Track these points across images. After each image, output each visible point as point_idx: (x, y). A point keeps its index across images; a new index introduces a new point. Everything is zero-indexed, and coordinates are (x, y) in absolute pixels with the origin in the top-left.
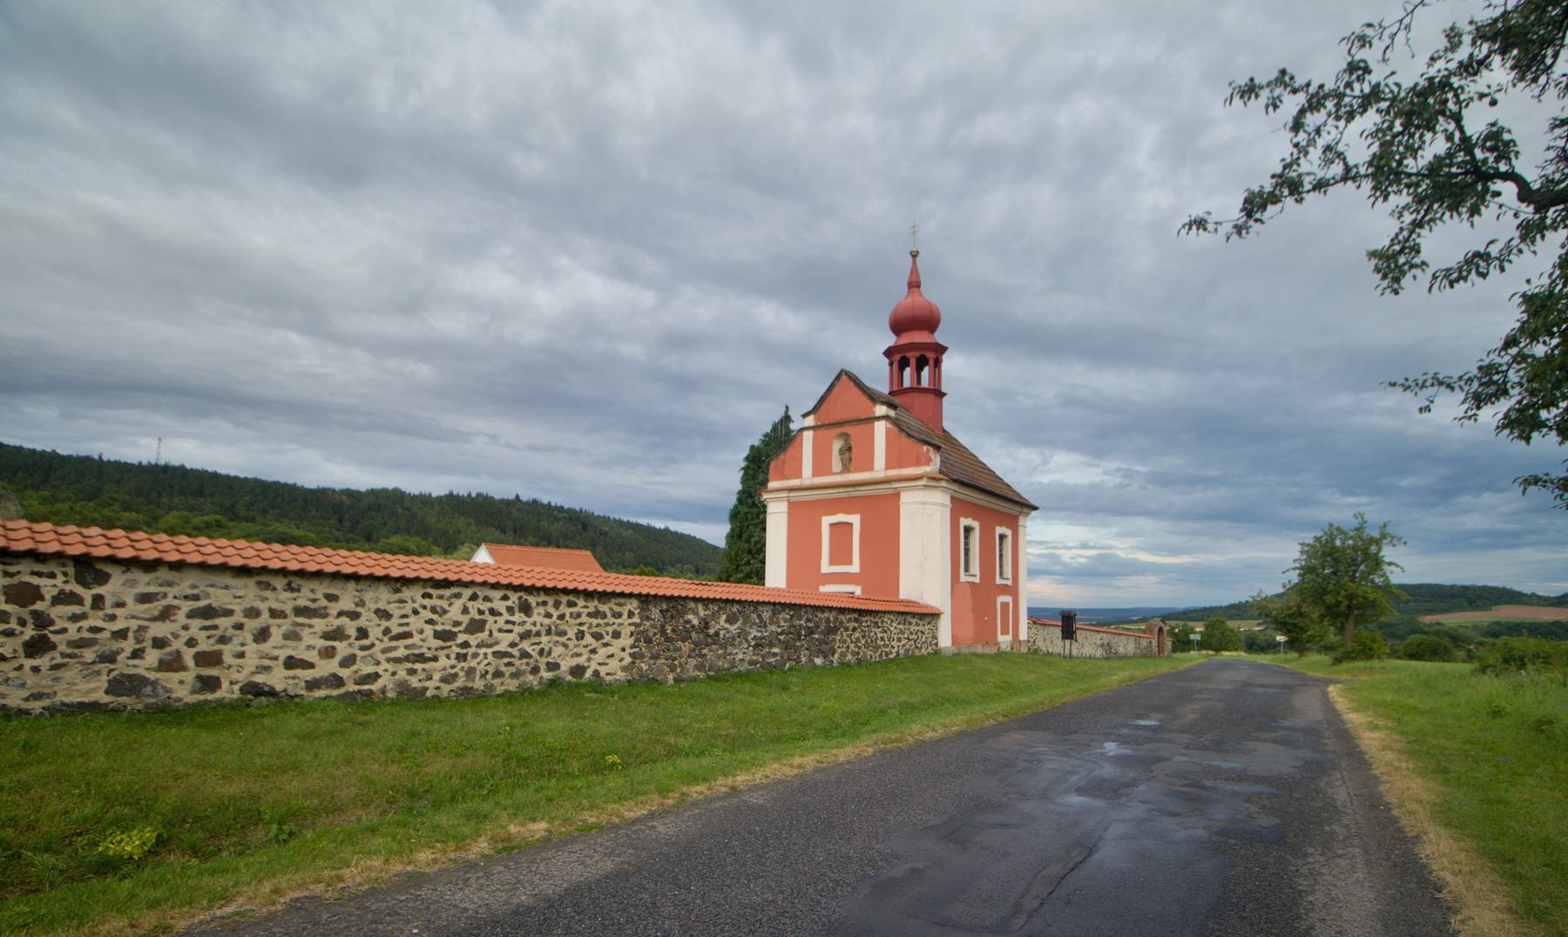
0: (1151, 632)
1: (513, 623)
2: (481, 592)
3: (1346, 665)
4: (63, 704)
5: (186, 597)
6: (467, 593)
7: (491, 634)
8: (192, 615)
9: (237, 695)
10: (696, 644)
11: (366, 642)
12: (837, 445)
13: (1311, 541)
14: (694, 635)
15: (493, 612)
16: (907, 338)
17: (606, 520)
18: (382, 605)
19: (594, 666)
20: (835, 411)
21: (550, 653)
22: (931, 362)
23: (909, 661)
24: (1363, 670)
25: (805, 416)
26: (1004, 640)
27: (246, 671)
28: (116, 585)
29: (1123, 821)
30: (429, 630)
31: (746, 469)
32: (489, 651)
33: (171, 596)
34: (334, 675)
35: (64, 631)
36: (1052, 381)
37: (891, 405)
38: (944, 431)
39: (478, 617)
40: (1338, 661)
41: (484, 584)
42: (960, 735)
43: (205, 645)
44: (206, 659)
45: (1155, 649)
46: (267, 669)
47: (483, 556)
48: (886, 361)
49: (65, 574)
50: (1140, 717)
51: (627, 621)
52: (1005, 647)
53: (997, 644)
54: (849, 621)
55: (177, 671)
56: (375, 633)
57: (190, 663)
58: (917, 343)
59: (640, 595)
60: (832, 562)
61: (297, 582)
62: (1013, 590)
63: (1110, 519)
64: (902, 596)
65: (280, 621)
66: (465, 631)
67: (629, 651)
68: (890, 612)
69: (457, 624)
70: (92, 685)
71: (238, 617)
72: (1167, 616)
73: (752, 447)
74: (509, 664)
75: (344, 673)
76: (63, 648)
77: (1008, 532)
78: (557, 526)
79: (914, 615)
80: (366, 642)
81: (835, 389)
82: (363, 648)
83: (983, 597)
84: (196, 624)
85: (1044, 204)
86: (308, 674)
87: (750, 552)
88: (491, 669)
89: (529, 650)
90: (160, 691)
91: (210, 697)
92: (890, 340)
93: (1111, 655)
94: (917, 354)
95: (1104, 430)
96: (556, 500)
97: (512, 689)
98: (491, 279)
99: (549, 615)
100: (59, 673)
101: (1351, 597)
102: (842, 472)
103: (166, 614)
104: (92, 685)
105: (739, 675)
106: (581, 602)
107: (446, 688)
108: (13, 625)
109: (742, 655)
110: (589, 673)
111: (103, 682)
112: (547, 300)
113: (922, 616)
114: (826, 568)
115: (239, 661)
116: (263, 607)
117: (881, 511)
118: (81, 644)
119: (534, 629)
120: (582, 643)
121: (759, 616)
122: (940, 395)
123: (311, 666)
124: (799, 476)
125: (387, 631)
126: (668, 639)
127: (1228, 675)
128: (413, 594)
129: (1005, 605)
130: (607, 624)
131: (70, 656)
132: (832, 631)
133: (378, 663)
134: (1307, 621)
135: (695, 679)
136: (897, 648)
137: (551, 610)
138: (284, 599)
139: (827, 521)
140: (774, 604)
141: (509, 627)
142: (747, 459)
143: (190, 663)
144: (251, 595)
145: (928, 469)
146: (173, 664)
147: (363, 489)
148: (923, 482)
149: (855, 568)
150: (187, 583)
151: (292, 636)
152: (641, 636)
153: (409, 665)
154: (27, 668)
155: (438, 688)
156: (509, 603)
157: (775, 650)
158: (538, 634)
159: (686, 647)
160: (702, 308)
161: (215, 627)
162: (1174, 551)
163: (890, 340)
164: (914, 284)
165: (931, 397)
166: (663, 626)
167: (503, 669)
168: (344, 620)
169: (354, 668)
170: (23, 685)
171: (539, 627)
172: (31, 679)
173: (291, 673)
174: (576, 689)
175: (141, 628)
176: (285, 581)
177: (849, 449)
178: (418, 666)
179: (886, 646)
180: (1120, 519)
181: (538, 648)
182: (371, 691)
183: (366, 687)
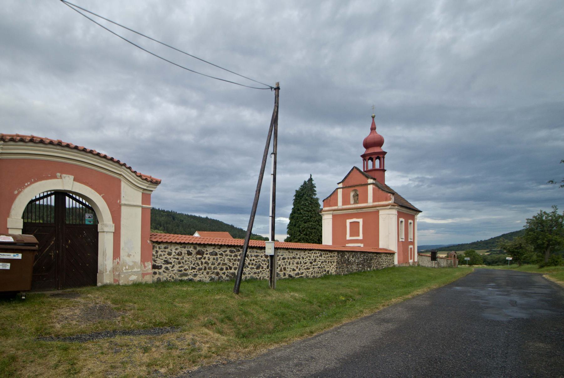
0: (451, 257)
3: (546, 268)
6: (314, 252)
12: (352, 194)
13: (531, 218)
20: (351, 182)
23: (387, 269)
24: (554, 270)
25: (338, 184)
26: (411, 261)
40: (542, 267)
47: (196, 235)
48: (362, 159)
52: (411, 264)
60: (351, 236)
62: (413, 243)
75: (299, 272)
77: (412, 221)
78: (163, 218)
81: (351, 174)
83: (405, 245)
85: (384, 43)
87: (300, 231)
92: (363, 151)
94: (376, 156)
98: (128, 111)
101: (549, 241)
102: (354, 204)
112: (151, 117)
114: (348, 237)
117: (372, 218)
124: (337, 205)
127: (11, 352)
128: (306, 252)
129: (411, 248)
132: (371, 260)
134: (524, 250)
136: (385, 265)
138: (292, 255)
139: (348, 221)
142: (296, 196)
145: (390, 202)
148: (389, 207)
152: (338, 262)
159: (345, 265)
160: (218, 115)
162: (444, 217)
163: (363, 151)
165: (382, 172)
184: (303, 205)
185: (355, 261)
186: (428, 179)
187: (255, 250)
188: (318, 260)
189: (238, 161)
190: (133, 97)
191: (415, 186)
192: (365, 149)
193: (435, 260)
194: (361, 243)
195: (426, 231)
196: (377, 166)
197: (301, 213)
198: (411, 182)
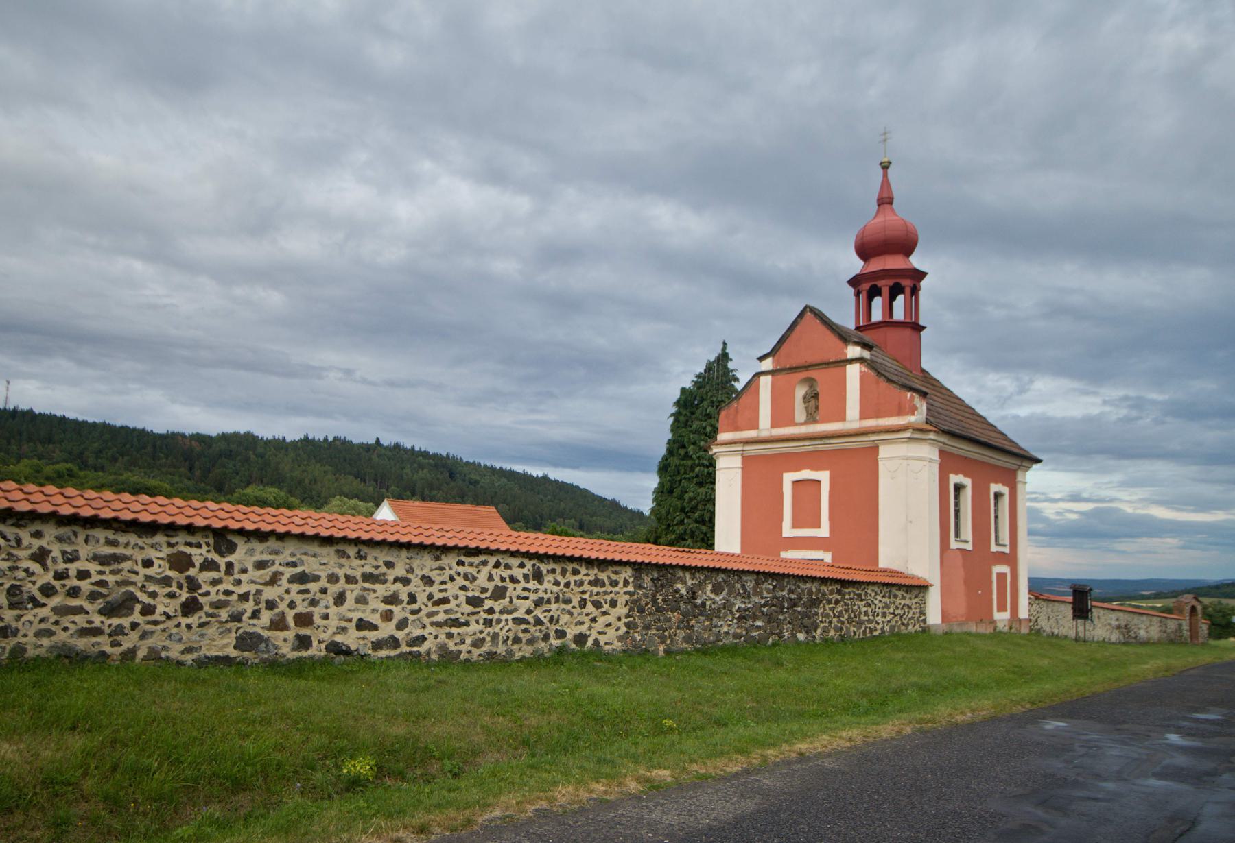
0: (1181, 612)
1: (529, 590)
2: (504, 560)
4: (206, 657)
5: (288, 564)
6: (492, 560)
7: (511, 601)
8: (292, 580)
9: (323, 653)
10: (684, 615)
11: (415, 607)
12: (801, 391)
14: (682, 604)
15: (513, 580)
16: (877, 265)
17: (475, 466)
18: (426, 572)
19: (594, 635)
21: (558, 621)
22: (908, 290)
23: (894, 639)
25: (761, 359)
26: (1001, 617)
27: (330, 632)
28: (242, 554)
29: (1217, 803)
30: (462, 599)
31: (676, 416)
32: (510, 617)
33: (277, 563)
34: (392, 637)
35: (207, 594)
36: (1029, 286)
37: (866, 346)
38: (923, 371)
39: (500, 584)
41: (507, 551)
42: (993, 720)
43: (301, 608)
44: (304, 620)
45: (1186, 634)
46: (344, 629)
47: (385, 513)
48: (851, 290)
49: (208, 545)
50: (1196, 710)
51: (622, 588)
53: (994, 622)
54: (832, 592)
55: (282, 630)
56: (421, 598)
57: (291, 623)
58: (887, 269)
59: (635, 563)
60: (795, 525)
61: (365, 550)
62: (1010, 559)
63: (1112, 462)
64: (883, 563)
65: (353, 586)
66: (490, 598)
67: (624, 620)
68: (874, 584)
69: (484, 590)
70: (225, 641)
71: (323, 583)
72: (1199, 590)
73: (683, 390)
74: (526, 631)
75: (400, 635)
76: (207, 608)
77: (1005, 490)
79: (899, 586)
80: (415, 607)
81: (798, 328)
82: (413, 612)
83: (975, 567)
84: (295, 587)
86: (373, 636)
87: (683, 510)
88: (511, 635)
89: (542, 617)
90: (271, 647)
91: (304, 654)
92: (856, 265)
93: (1129, 638)
94: (891, 282)
95: (1100, 348)
96: (420, 445)
97: (528, 655)
98: (345, 191)
99: (557, 583)
100: (204, 630)
102: (805, 423)
103: (274, 580)
104: (225, 641)
105: (724, 649)
106: (583, 570)
107: (476, 652)
108: (174, 588)
109: (727, 626)
110: (590, 642)
111: (232, 639)
112: (408, 211)
113: (909, 588)
114: (788, 531)
115: (325, 622)
116: (341, 573)
117: (856, 467)
118: (218, 605)
119: (546, 597)
120: (585, 611)
121: (743, 586)
122: (918, 328)
123: (375, 628)
124: (755, 426)
125: (430, 597)
126: (659, 610)
128: (449, 560)
129: (1001, 576)
130: (606, 593)
131: (211, 615)
132: (814, 603)
133: (424, 627)
135: (682, 652)
136: (882, 624)
137: (559, 578)
138: (355, 567)
139: (788, 478)
140: (758, 573)
141: (526, 594)
142: (678, 403)
143: (291, 623)
144: (332, 563)
145: (912, 419)
146: (278, 624)
147: (214, 433)
148: (908, 434)
149: (824, 531)
150: (289, 551)
151: (361, 600)
152: (635, 606)
153: (447, 630)
154: (183, 625)
155: (469, 652)
156: (525, 571)
157: (759, 623)
158: (549, 602)
159: (675, 617)
160: (586, 213)
161: (307, 591)
163: (856, 265)
164: (885, 200)
165: (908, 332)
166: (654, 596)
167: (521, 635)
168: (398, 586)
169: (407, 631)
170: (180, 640)
171: (549, 595)
172: (186, 635)
173: (362, 634)
174: (581, 656)
175: (259, 592)
176: (356, 550)
177: (816, 396)
178: (454, 630)
179: (869, 621)
180: (1126, 462)
181: (548, 615)
182: (419, 654)
183: (415, 649)
184: (696, 431)
185: (727, 605)
186: (1154, 402)
187: (101, 534)
188: (513, 590)
189: (640, 333)
190: (362, 156)
191: (1120, 420)
192: (862, 263)
193: (1086, 618)
194: (826, 550)
195: (1156, 540)
196: (899, 314)
197: (687, 456)
198: (1107, 409)
